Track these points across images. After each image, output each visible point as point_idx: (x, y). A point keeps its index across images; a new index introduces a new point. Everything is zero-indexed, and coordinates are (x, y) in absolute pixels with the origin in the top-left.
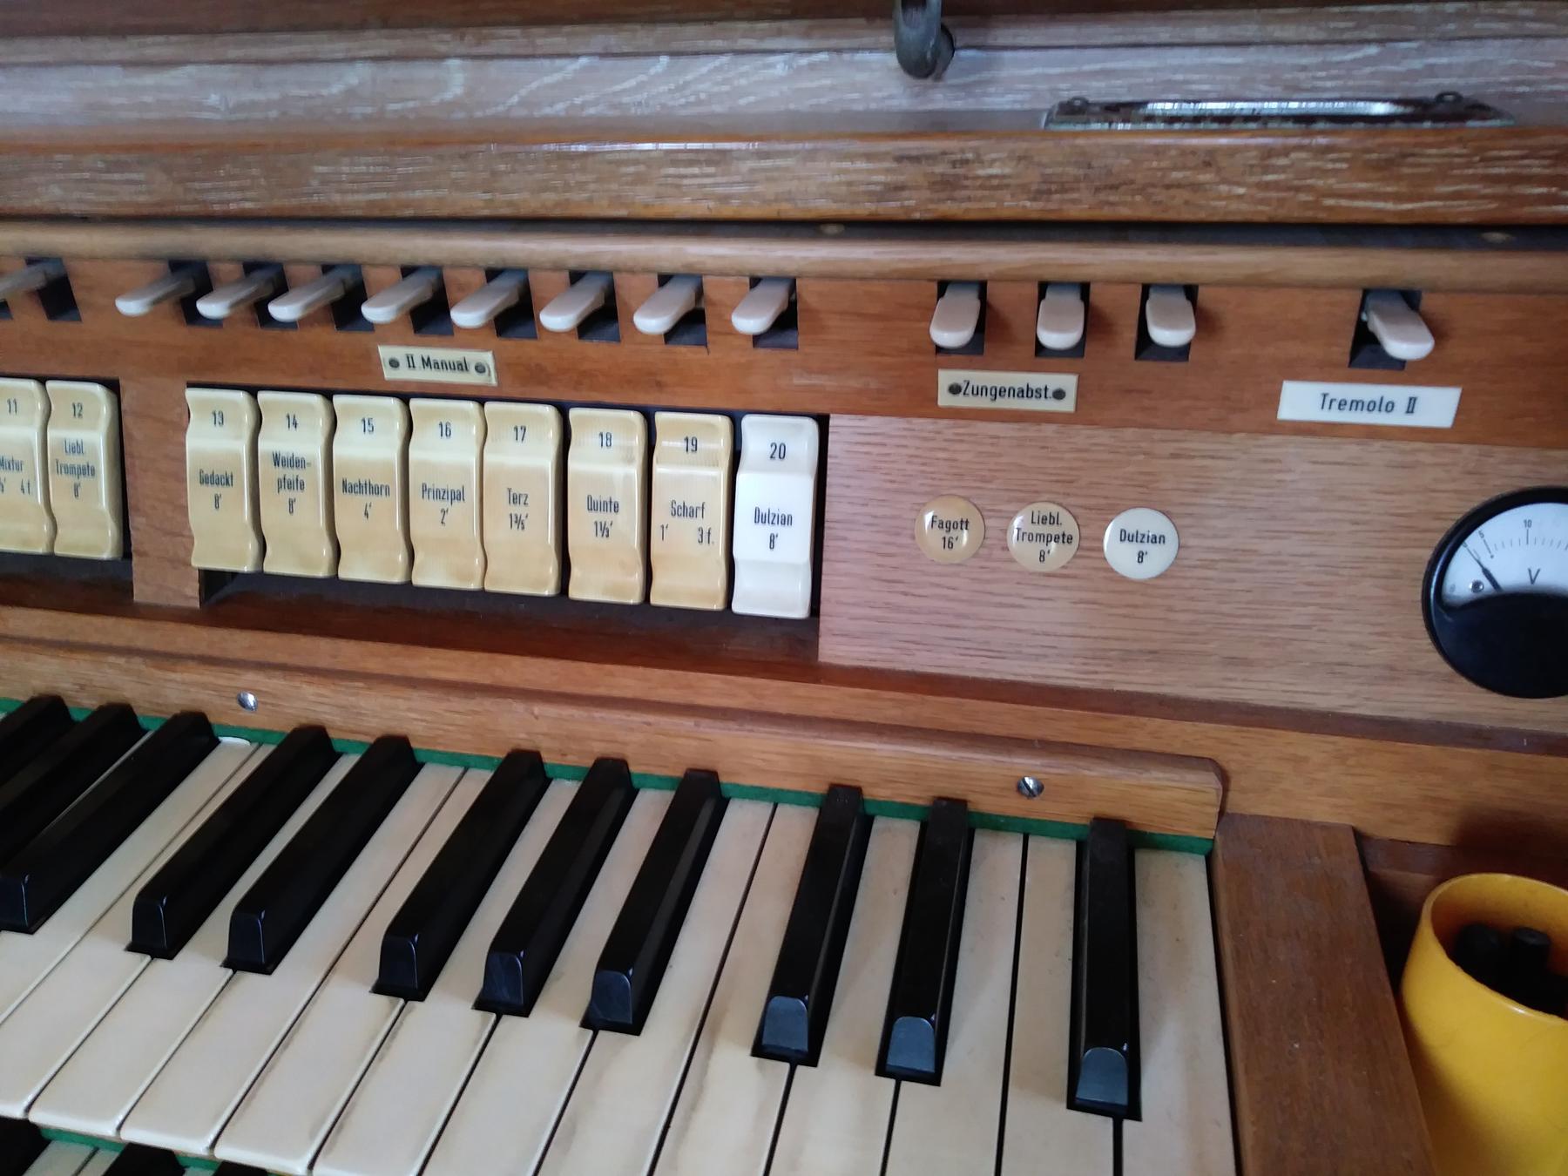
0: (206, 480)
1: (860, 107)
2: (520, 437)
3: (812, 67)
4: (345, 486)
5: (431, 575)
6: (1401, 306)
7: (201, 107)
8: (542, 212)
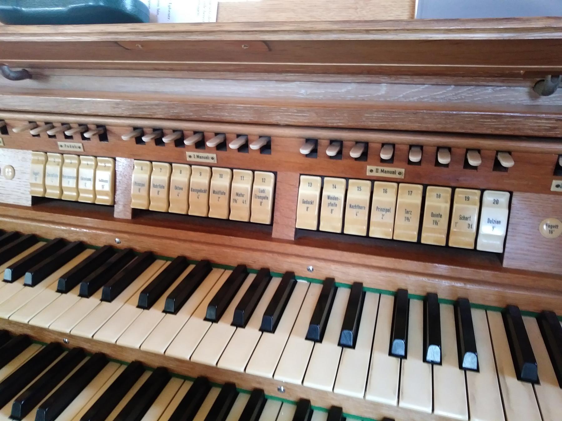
0: (304, 202)
1: (513, 103)
2: (410, 194)
3: (500, 90)
4: (214, 192)
5: (375, 233)
6: (507, 155)
7: (298, 93)
8: (436, 130)
